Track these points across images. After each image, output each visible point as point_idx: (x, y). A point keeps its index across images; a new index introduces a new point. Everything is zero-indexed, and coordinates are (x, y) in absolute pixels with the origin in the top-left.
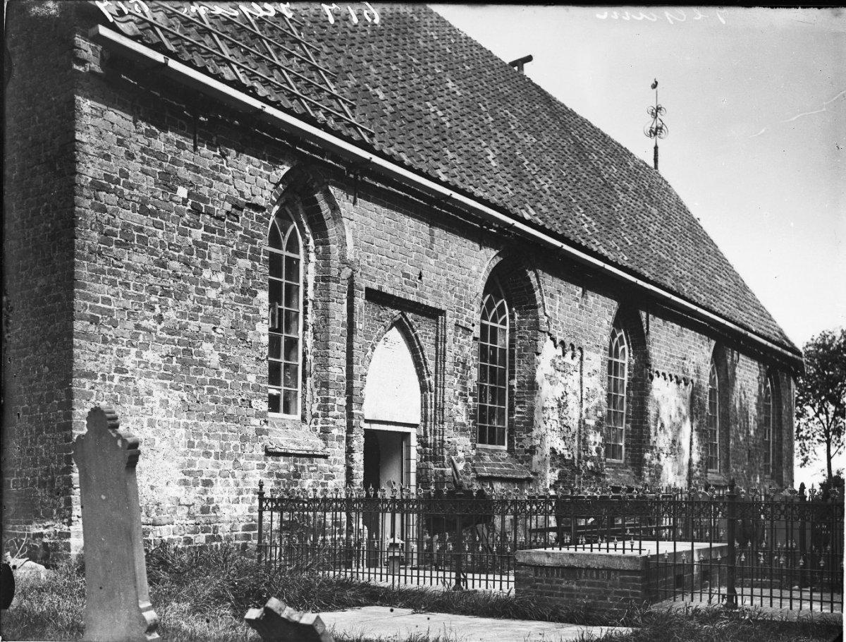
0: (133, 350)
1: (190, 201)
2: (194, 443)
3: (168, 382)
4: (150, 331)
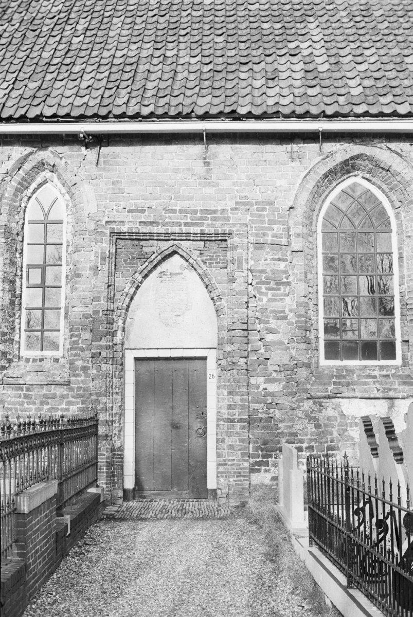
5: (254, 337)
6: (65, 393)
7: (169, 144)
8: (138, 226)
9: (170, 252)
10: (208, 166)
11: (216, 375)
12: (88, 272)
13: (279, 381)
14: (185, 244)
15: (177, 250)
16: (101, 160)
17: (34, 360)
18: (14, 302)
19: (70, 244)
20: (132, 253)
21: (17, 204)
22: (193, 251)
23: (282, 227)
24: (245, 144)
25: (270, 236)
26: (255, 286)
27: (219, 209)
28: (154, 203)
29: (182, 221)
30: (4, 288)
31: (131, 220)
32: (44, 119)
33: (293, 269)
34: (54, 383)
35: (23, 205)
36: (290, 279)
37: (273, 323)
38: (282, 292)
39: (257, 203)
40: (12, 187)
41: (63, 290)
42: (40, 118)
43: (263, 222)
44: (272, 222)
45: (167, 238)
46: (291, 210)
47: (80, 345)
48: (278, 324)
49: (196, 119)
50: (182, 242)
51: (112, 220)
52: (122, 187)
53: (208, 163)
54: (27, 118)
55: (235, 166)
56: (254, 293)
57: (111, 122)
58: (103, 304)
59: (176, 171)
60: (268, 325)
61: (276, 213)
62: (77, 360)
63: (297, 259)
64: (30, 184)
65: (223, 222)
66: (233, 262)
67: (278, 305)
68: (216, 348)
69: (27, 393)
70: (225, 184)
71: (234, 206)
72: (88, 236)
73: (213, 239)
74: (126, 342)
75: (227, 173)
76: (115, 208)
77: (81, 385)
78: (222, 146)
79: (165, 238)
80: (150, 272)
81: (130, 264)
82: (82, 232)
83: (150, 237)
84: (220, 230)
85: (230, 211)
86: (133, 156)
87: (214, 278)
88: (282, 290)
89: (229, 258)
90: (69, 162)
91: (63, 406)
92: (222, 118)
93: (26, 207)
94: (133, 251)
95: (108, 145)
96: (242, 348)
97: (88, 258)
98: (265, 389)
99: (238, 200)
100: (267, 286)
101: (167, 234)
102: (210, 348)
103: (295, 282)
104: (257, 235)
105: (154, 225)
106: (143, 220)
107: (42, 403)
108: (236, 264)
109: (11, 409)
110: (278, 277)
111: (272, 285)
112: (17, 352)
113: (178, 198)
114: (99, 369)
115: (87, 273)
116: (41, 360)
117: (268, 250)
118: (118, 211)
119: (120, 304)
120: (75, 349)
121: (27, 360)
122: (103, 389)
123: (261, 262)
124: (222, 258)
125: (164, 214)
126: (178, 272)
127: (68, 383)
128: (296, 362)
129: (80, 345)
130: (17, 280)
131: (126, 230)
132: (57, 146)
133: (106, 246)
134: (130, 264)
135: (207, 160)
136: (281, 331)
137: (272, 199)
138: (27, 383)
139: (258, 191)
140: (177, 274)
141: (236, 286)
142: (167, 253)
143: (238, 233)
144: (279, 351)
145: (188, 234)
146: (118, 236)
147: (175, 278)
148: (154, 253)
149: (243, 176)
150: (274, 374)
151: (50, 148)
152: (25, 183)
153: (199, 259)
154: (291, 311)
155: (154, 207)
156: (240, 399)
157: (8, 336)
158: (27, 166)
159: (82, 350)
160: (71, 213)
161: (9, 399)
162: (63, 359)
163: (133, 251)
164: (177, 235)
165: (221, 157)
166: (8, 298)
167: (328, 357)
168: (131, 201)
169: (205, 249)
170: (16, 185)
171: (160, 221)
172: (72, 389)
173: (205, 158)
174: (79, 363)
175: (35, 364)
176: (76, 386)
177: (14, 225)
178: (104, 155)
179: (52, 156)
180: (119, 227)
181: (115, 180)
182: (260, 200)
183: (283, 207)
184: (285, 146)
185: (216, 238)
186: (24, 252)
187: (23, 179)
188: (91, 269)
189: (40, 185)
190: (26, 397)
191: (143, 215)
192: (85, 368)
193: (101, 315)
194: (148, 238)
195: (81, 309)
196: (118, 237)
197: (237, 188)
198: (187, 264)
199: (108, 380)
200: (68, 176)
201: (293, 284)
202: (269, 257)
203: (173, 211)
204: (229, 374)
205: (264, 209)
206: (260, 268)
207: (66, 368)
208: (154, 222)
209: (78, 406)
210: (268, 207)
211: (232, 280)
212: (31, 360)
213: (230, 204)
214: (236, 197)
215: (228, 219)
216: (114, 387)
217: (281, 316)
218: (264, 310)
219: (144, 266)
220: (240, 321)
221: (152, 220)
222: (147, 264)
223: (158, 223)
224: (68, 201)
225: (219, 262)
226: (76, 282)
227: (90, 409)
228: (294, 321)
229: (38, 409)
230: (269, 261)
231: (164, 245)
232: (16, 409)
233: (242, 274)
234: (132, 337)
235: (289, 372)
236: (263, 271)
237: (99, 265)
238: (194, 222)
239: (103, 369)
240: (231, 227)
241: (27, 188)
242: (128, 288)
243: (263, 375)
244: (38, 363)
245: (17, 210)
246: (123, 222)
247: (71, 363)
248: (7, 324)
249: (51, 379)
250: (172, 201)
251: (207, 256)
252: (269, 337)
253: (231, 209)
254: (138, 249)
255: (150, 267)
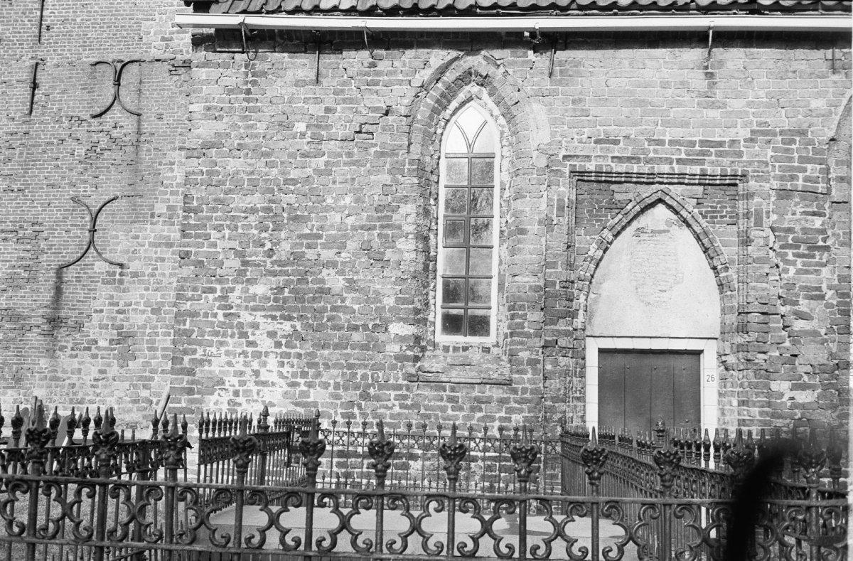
0: (239, 287)
1: (309, 133)
2: (307, 373)
3: (278, 314)
4: (259, 265)
5: (776, 323)
6: (505, 396)
7: (654, 47)
8: (609, 162)
9: (653, 200)
10: (711, 78)
11: (716, 377)
12: (537, 226)
13: (813, 387)
14: (676, 190)
15: (663, 198)
16: (557, 69)
17: (456, 349)
18: (428, 265)
19: (507, 188)
20: (598, 201)
21: (432, 130)
22: (687, 200)
23: (818, 167)
24: (763, 48)
25: (801, 180)
26: (778, 251)
27: (727, 140)
28: (632, 131)
29: (674, 157)
30: (417, 247)
31: (599, 154)
32: (478, 10)
33: (833, 227)
34: (490, 381)
35: (439, 131)
36: (829, 243)
37: (804, 305)
38: (817, 259)
39: (781, 133)
40: (427, 105)
41: (495, 251)
42: (474, 9)
43: (791, 159)
44: (803, 160)
45: (651, 180)
46: (832, 142)
47: (526, 329)
48: (812, 306)
49: (695, 12)
50: (671, 187)
51: (572, 154)
52: (587, 107)
53: (712, 73)
54: (454, 8)
55: (750, 79)
56: (776, 261)
57: (572, 15)
58: (559, 272)
59: (665, 85)
60: (796, 308)
61: (810, 147)
62: (521, 350)
63: (839, 213)
64: (449, 102)
65: (733, 159)
66: (747, 215)
67: (810, 280)
68: (716, 339)
69: (452, 394)
70: (736, 104)
71: (749, 136)
72: (535, 176)
73: (718, 182)
74: (588, 327)
75: (739, 89)
76: (576, 137)
77: (527, 385)
78: (731, 50)
79: (648, 180)
80: (624, 228)
81: (597, 216)
82: (527, 171)
83: (628, 178)
84: (729, 169)
85: (742, 142)
86: (602, 64)
87: (717, 239)
88: (818, 257)
89: (741, 211)
90: (510, 71)
91: (503, 414)
92: (735, 11)
93: (442, 134)
94: (600, 198)
95: (565, 48)
96: (760, 339)
97: (535, 207)
98: (792, 398)
99: (755, 128)
100: (795, 251)
101: (652, 174)
102: (709, 338)
103: (837, 246)
104: (782, 178)
105: (633, 161)
106: (616, 154)
107: (473, 409)
108: (753, 219)
109: (428, 417)
110: (812, 238)
111: (803, 249)
112: (432, 337)
113: (666, 124)
114: (555, 363)
115: (534, 228)
116: (465, 349)
117: (797, 200)
118: (580, 142)
119: (582, 273)
120: (519, 334)
121: (446, 349)
122: (562, 392)
123: (786, 217)
124: (729, 209)
125: (646, 146)
126: (662, 229)
127: (508, 383)
128: (837, 362)
129: (526, 329)
130: (432, 236)
131: (592, 168)
132: (493, 49)
133: (565, 190)
134: (597, 216)
135: (709, 70)
136: (815, 316)
137: (805, 126)
138: (452, 380)
139: (784, 115)
140: (660, 232)
141: (753, 251)
142: (649, 201)
143: (755, 174)
144: (813, 345)
145: (682, 175)
146: (580, 176)
147: (658, 237)
148: (631, 201)
149: (762, 93)
150: (806, 378)
151: (483, 52)
152: (444, 101)
153: (696, 211)
154: (830, 288)
155: (632, 136)
156: (759, 412)
157: (421, 315)
158: (449, 77)
159: (528, 336)
160: (507, 144)
161: (426, 402)
162: (496, 349)
163: (600, 198)
164: (665, 176)
165: (730, 65)
166: (422, 261)
167: (487, 333)
168: (598, 127)
169: (705, 196)
170: (433, 103)
171: (642, 156)
172: (515, 391)
173: (707, 68)
174: (524, 355)
175: (456, 354)
176: (521, 386)
177: (427, 159)
178: (560, 61)
179: (484, 63)
180: (583, 164)
181: (576, 97)
182: (787, 128)
183: (821, 138)
184: (822, 51)
185: (723, 182)
186: (439, 198)
187: (443, 95)
188: (540, 222)
189: (463, 104)
190: (451, 399)
191: (616, 147)
192: (533, 363)
193: (557, 287)
194: (623, 179)
195: (526, 279)
196: (580, 178)
197: (753, 110)
198: (675, 217)
199: (568, 379)
200: (508, 93)
201: (833, 249)
202: (799, 210)
203: (661, 142)
204: (741, 376)
205: (793, 141)
206: (786, 225)
207: (503, 361)
208: (633, 158)
209: (523, 414)
210: (798, 139)
211: (746, 241)
212: (451, 349)
213: (744, 133)
214: (751, 122)
215: (740, 154)
216: (574, 389)
217: (816, 295)
218: (790, 286)
219: (616, 220)
220: (759, 300)
221: (629, 155)
222: (620, 216)
223: (639, 158)
224: (502, 126)
225: (725, 216)
226: (519, 242)
227: (540, 419)
228: (835, 303)
229: (467, 418)
230: (798, 216)
231: (646, 192)
232: (436, 416)
233: (761, 233)
234: (597, 320)
235: (827, 375)
236: (790, 230)
237: (554, 217)
238: (691, 157)
239: (562, 364)
240: (744, 166)
241: (445, 108)
242: (594, 250)
243: (790, 378)
244: (461, 353)
245: (432, 139)
246: (588, 156)
247: (512, 355)
248: (420, 298)
249: (486, 376)
250: (659, 127)
251: (708, 207)
252: (799, 325)
253: (745, 140)
254: (606, 195)
255: (625, 221)
